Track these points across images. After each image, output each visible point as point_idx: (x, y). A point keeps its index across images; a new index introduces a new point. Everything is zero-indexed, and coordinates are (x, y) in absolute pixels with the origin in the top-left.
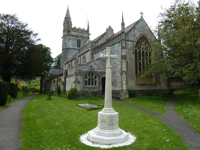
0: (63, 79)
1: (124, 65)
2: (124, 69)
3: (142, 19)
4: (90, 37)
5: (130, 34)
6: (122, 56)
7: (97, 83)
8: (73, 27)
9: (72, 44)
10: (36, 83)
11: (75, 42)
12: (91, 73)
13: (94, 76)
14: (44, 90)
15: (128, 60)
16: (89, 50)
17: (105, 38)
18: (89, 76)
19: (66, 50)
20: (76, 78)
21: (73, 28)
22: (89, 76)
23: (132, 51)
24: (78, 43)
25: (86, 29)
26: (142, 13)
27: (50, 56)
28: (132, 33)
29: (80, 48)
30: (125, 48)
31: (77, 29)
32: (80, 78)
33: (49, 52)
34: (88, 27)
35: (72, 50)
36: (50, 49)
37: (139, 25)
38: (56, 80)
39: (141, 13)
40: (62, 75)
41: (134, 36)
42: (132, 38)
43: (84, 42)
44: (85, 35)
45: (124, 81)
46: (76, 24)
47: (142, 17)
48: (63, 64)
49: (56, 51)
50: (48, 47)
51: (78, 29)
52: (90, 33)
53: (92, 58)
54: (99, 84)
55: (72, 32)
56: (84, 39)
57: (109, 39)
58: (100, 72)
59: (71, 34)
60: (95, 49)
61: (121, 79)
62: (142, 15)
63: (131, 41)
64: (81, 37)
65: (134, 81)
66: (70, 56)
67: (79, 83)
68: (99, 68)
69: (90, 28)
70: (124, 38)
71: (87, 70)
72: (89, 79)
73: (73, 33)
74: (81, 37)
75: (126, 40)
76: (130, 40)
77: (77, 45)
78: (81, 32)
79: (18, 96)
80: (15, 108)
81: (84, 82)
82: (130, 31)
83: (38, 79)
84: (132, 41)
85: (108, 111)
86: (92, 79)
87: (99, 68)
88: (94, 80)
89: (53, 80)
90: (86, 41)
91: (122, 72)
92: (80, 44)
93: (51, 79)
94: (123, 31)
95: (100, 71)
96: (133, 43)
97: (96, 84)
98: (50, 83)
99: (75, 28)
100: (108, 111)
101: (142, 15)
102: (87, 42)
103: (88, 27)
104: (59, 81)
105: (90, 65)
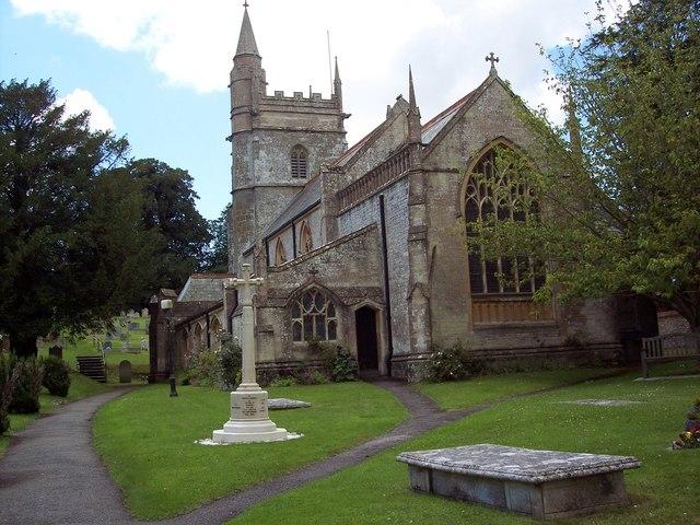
0: (223, 319)
1: (420, 261)
2: (421, 278)
3: (493, 81)
4: (346, 129)
5: (443, 147)
6: (413, 231)
7: (339, 330)
8: (270, 92)
9: (270, 166)
10: (129, 337)
11: (283, 159)
12: (314, 297)
13: (326, 306)
14: (164, 371)
15: (433, 242)
16: (319, 202)
17: (380, 149)
18: (307, 307)
19: (248, 192)
20: (258, 318)
21: (272, 99)
22: (307, 307)
23: (452, 209)
24: (294, 158)
25: (327, 95)
26: (492, 59)
27: (189, 208)
28: (453, 139)
29: (305, 181)
30: (425, 202)
31: (286, 99)
32: (272, 319)
33: (187, 191)
34: (337, 84)
35: (270, 194)
36: (190, 179)
37: (481, 104)
38: (203, 326)
39: (487, 59)
40: (219, 305)
41: (462, 150)
42: (452, 160)
43: (324, 153)
44: (325, 122)
45: (419, 320)
46: (282, 78)
47: (493, 72)
48: (237, 253)
49: (212, 200)
50: (178, 170)
51: (292, 100)
52: (345, 110)
53: (332, 233)
54: (346, 332)
55: (265, 115)
56: (322, 141)
57: (405, 149)
58: (350, 290)
59: (263, 125)
60: (340, 196)
61: (410, 313)
62: (493, 67)
63: (448, 171)
64: (307, 131)
65: (466, 316)
66: (262, 221)
67: (271, 333)
68: (346, 274)
69: (344, 88)
70: (417, 163)
71: (298, 285)
72: (308, 319)
73: (270, 120)
74: (307, 131)
75: (424, 171)
76: (444, 166)
77: (289, 168)
78: (307, 110)
79: (71, 392)
80: (61, 433)
81: (286, 331)
82: (442, 135)
83: (143, 320)
84: (455, 171)
85: (249, 387)
86: (321, 319)
87: (346, 274)
88: (328, 320)
89: (194, 327)
90: (332, 147)
91: (413, 286)
92: (304, 167)
93: (187, 322)
94: (414, 138)
95: (347, 285)
96: (456, 176)
97: (333, 336)
98: (185, 336)
99: (279, 94)
100: (249, 387)
101: (493, 67)
102: (334, 151)
103: (337, 84)
104: (214, 328)
105: (306, 267)
